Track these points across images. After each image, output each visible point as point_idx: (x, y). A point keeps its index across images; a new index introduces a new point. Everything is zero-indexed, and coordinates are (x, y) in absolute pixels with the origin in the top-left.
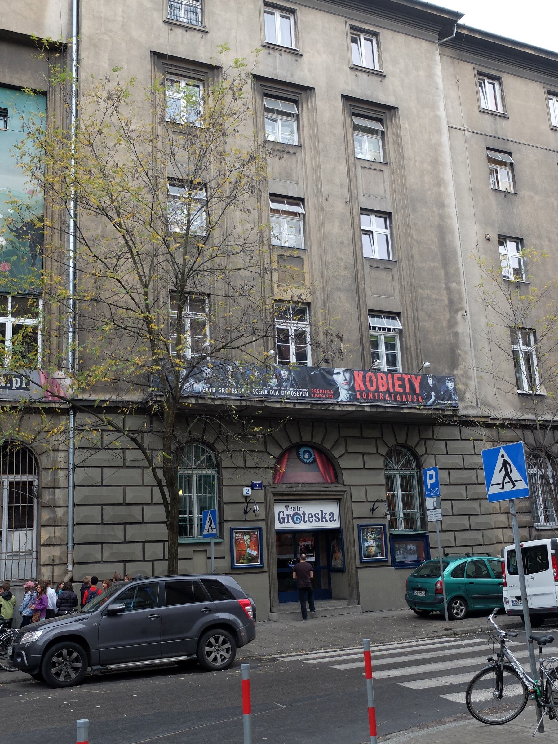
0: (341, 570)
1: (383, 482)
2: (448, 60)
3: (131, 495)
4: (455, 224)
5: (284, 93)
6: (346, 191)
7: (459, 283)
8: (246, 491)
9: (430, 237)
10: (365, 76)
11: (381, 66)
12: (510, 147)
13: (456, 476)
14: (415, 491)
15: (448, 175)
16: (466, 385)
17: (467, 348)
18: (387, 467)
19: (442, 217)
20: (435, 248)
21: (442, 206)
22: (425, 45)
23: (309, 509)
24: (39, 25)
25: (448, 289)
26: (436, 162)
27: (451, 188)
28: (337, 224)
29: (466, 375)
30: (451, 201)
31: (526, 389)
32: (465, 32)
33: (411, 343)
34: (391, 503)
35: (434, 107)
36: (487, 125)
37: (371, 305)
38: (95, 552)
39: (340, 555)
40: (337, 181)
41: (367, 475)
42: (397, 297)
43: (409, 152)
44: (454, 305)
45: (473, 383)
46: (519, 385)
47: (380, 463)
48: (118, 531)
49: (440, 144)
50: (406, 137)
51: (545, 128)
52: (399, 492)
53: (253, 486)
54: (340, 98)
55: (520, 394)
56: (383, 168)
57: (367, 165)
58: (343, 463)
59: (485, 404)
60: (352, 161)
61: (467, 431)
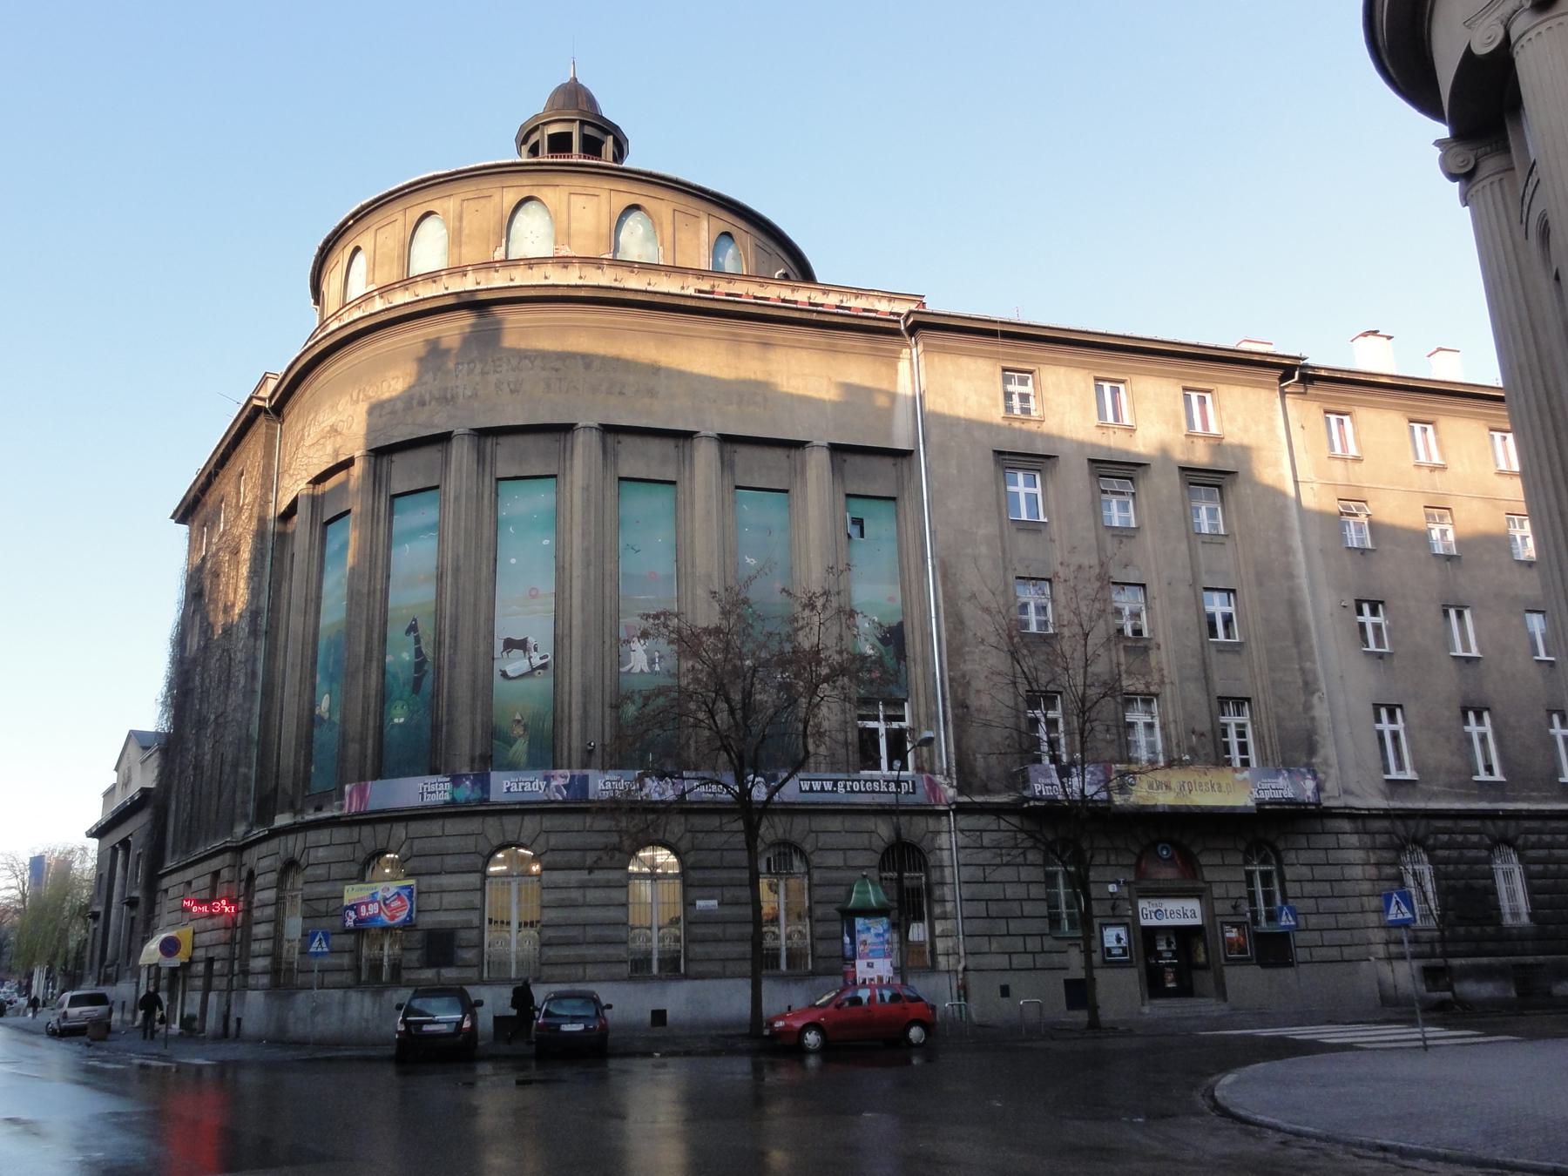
0: (1205, 967)
1: (1243, 878)
3: (1010, 891)
6: (1189, 574)
7: (1314, 662)
8: (1112, 888)
12: (1366, 495)
13: (1319, 872)
14: (1276, 887)
18: (1247, 862)
19: (1292, 590)
21: (1290, 576)
22: (1264, 394)
23: (1170, 905)
24: (889, 435)
25: (1303, 670)
27: (1300, 556)
29: (1326, 762)
30: (1301, 570)
31: (1372, 647)
34: (1253, 902)
38: (983, 944)
39: (1201, 948)
41: (1227, 874)
44: (1309, 687)
47: (1239, 859)
53: (1118, 883)
55: (1388, 781)
58: (1203, 860)
59: (1347, 792)
60: (1192, 535)
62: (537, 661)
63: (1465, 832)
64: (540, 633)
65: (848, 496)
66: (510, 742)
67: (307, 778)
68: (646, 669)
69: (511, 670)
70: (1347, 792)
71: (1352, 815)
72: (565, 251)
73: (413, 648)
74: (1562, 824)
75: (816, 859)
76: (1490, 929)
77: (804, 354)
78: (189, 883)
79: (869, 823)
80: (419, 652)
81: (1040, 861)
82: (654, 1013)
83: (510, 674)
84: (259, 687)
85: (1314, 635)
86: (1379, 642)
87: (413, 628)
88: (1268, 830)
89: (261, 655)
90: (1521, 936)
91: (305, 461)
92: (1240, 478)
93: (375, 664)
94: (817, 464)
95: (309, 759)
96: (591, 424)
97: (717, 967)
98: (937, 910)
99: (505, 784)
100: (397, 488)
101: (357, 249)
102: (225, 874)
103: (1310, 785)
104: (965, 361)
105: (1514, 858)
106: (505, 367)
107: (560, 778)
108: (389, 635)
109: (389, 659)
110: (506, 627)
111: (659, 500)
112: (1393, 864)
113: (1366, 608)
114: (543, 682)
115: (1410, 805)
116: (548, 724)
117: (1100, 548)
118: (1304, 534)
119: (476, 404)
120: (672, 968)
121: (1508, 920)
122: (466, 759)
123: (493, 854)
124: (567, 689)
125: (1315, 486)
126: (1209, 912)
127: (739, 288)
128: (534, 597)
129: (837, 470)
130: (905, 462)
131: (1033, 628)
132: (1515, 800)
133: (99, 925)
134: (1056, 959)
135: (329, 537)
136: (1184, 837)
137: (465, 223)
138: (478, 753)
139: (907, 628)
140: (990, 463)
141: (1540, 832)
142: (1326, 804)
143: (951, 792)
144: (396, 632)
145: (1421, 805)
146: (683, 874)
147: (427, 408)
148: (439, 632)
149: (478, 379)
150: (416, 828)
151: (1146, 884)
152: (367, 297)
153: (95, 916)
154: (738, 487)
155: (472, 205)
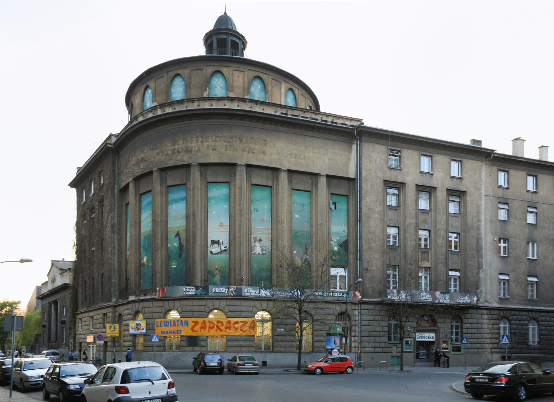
2: (487, 166)
4: (483, 236)
5: (428, 190)
6: (445, 226)
7: (482, 259)
9: (473, 242)
10: (455, 180)
11: (462, 175)
15: (483, 217)
16: (481, 295)
17: (483, 282)
20: (475, 246)
21: (479, 229)
22: (479, 163)
25: (478, 261)
26: (478, 212)
28: (441, 239)
29: (481, 292)
30: (483, 228)
31: (502, 254)
32: (496, 155)
33: (462, 281)
34: (452, 332)
35: (480, 189)
36: (500, 193)
37: (450, 268)
40: (442, 223)
41: (445, 325)
42: (459, 264)
43: (469, 209)
44: (480, 267)
45: (483, 295)
46: (499, 294)
47: (450, 321)
48: (373, 339)
49: (481, 205)
50: (468, 203)
51: (524, 191)
52: (454, 330)
53: (411, 327)
54: (445, 190)
56: (459, 216)
57: (453, 215)
58: (438, 321)
59: (487, 301)
60: (448, 214)
61: (480, 311)
62: (223, 248)
63: (522, 316)
64: (224, 238)
65: (331, 194)
66: (214, 275)
67: (140, 284)
68: (260, 253)
69: (214, 251)
70: (487, 301)
71: (487, 309)
72: (231, 95)
73: (178, 242)
74: (553, 314)
75: (315, 317)
76: (525, 346)
77: (319, 140)
78: (92, 317)
79: (333, 306)
80: (180, 243)
81: (387, 319)
82: (263, 362)
83: (214, 252)
84: (116, 252)
85: (483, 249)
86: (505, 253)
87: (178, 235)
88: (458, 312)
89: (116, 240)
90: (534, 348)
91: (131, 170)
92: (467, 194)
93: (164, 247)
94: (323, 181)
95: (140, 278)
96: (242, 164)
97: (283, 349)
98: (353, 334)
99: (214, 290)
100: (170, 183)
101: (147, 87)
102: (110, 315)
103: (475, 299)
104: (377, 146)
105: (508, 324)
106: (210, 140)
107: (233, 288)
108: (169, 237)
109: (169, 245)
110: (212, 235)
111: (264, 194)
112: (498, 324)
113: (502, 241)
114: (225, 256)
115: (506, 306)
116: (227, 270)
117: (417, 217)
118: (485, 214)
119: (200, 154)
120: (269, 349)
121: (531, 343)
122: (200, 281)
123: (212, 310)
124: (233, 258)
125: (491, 197)
126: (437, 337)
127: (308, 115)
128: (222, 226)
129: (329, 185)
130: (314, 178)
131: (391, 244)
132: (540, 306)
133: (46, 329)
134: (389, 349)
135: (143, 200)
136: (431, 314)
137: (192, 80)
138: (203, 279)
139: (349, 242)
140: (382, 185)
141: (546, 317)
142: (479, 305)
143: (360, 297)
144: (172, 236)
145: (510, 306)
146: (272, 320)
147: (181, 154)
148: (187, 235)
149: (200, 144)
150: (184, 303)
151: (420, 328)
152: (154, 109)
153: (44, 326)
154: (293, 189)
155: (195, 72)
